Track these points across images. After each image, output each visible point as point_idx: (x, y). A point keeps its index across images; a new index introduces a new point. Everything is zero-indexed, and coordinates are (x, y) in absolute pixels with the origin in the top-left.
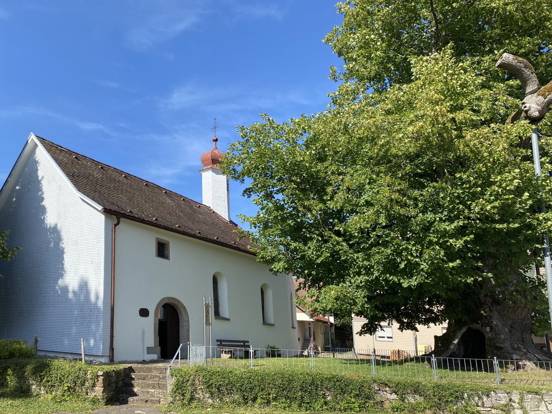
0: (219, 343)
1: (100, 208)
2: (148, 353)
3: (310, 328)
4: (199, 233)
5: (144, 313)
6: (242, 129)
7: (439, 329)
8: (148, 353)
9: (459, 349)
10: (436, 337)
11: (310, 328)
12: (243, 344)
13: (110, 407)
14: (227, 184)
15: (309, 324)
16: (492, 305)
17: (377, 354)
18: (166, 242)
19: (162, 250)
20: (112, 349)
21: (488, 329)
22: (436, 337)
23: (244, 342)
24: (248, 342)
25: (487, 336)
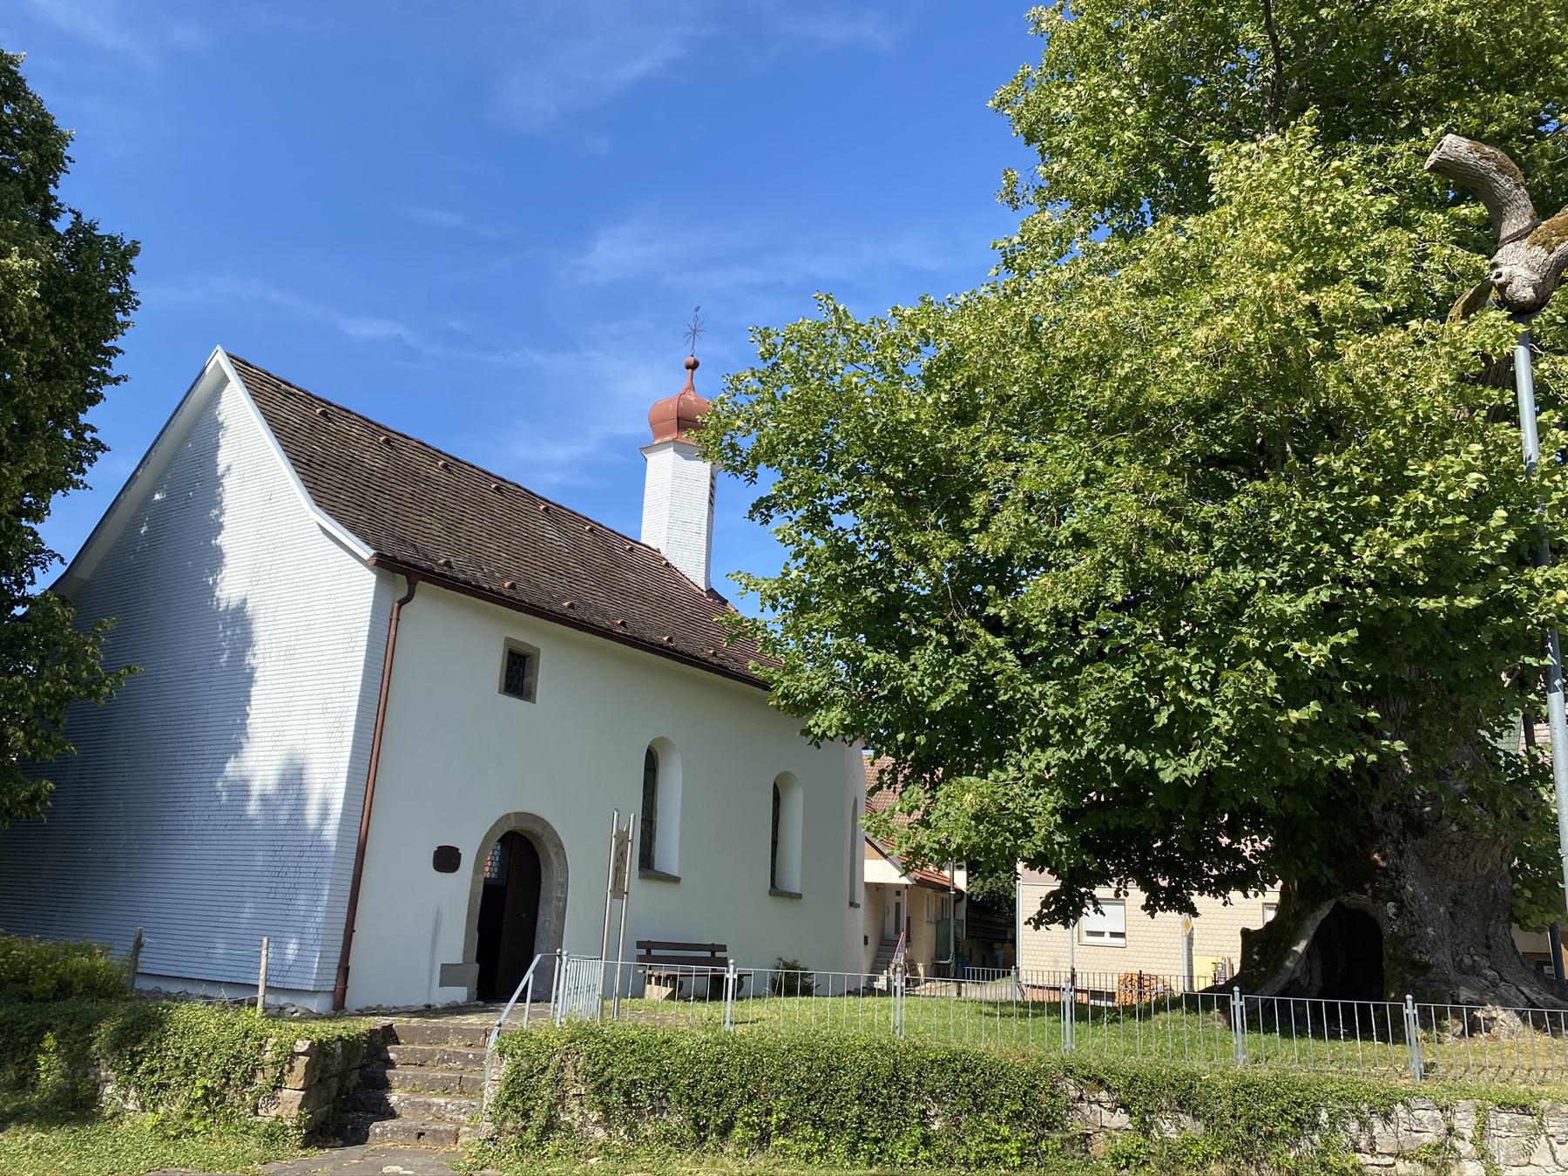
1: (367, 553)
3: (898, 905)
4: (623, 624)
5: (447, 859)
7: (1254, 909)
10: (1246, 933)
11: (898, 905)
14: (712, 486)
16: (1404, 834)
20: (344, 970)
21: (1391, 908)
22: (1246, 933)
23: (713, 948)
24: (723, 948)
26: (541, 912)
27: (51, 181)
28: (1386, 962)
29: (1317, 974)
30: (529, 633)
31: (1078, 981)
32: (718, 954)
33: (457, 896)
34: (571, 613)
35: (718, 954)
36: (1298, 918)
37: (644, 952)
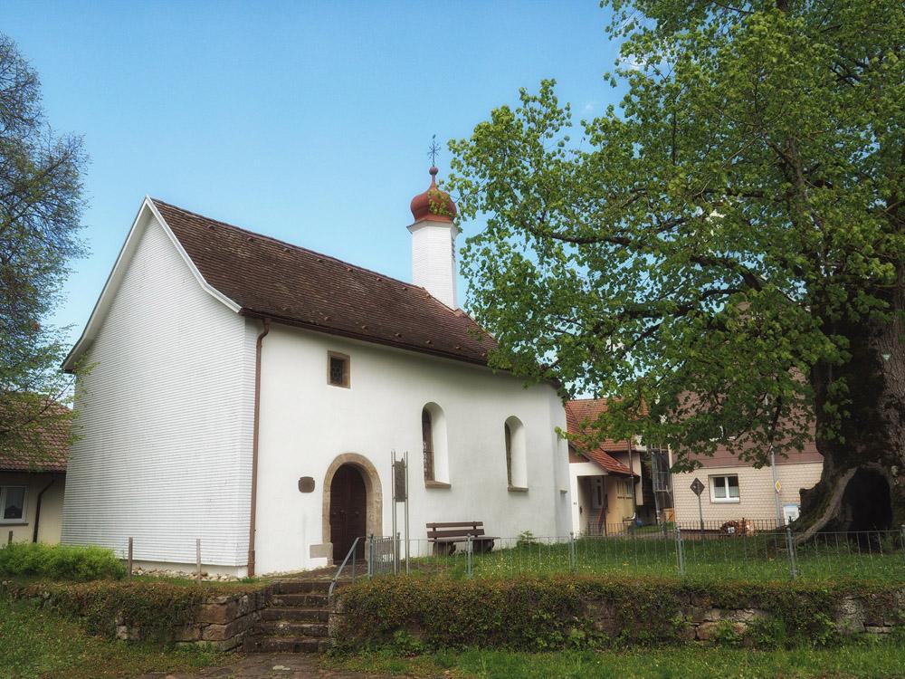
0: (431, 530)
1: (236, 308)
2: (312, 556)
3: (599, 488)
4: (400, 336)
5: (306, 485)
6: (583, 124)
7: (808, 473)
8: (312, 556)
9: (844, 512)
10: (803, 492)
11: (599, 488)
12: (472, 528)
13: (740, 485)
14: (453, 245)
15: (599, 481)
16: (900, 422)
17: (705, 528)
18: (344, 358)
19: (338, 373)
20: (252, 554)
21: (894, 469)
22: (803, 492)
23: (475, 524)
24: (481, 524)
25: (893, 483)
26: (368, 511)
27: (21, 550)
28: (892, 504)
29: (849, 513)
30: (11, 529)
31: (705, 525)
32: (477, 528)
33: (317, 501)
34: (366, 332)
35: (477, 528)
36: (834, 480)
37: (431, 530)
